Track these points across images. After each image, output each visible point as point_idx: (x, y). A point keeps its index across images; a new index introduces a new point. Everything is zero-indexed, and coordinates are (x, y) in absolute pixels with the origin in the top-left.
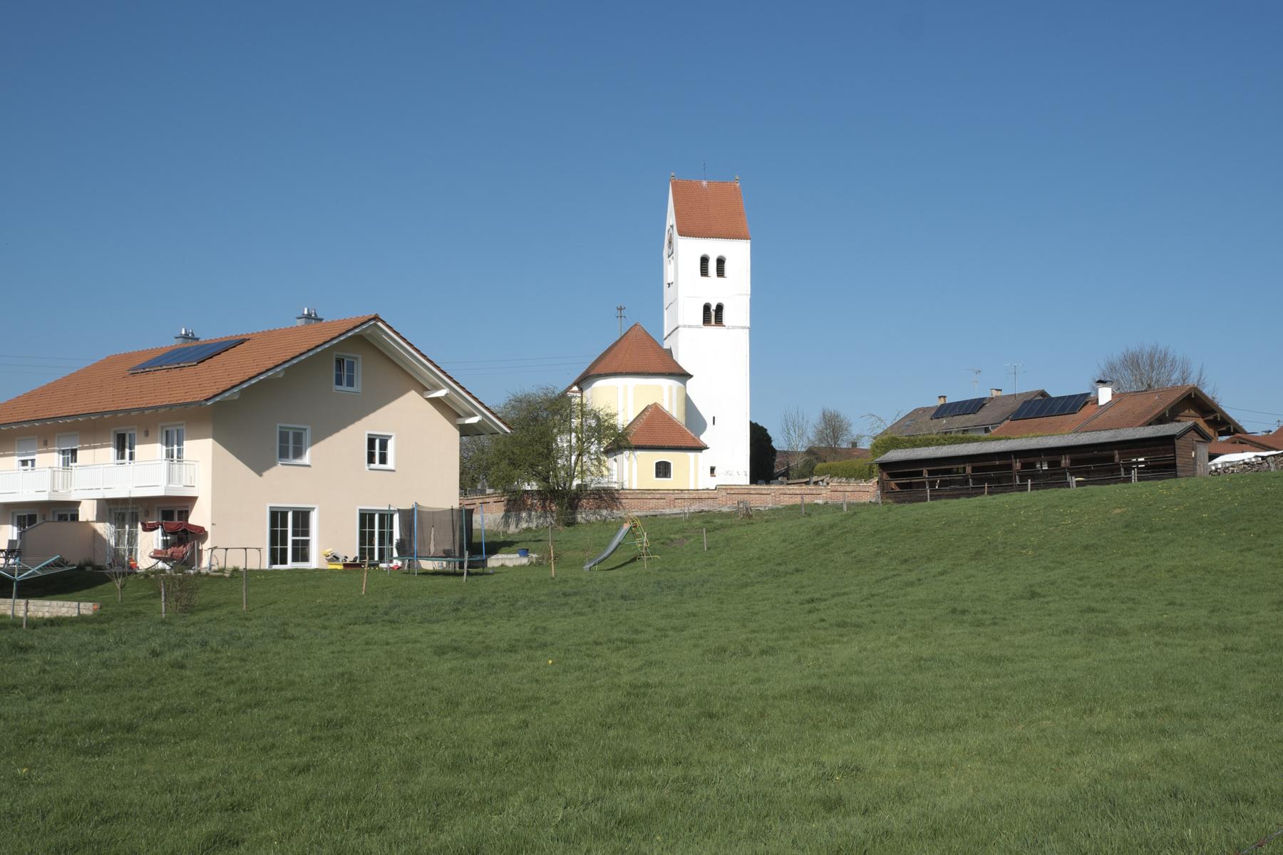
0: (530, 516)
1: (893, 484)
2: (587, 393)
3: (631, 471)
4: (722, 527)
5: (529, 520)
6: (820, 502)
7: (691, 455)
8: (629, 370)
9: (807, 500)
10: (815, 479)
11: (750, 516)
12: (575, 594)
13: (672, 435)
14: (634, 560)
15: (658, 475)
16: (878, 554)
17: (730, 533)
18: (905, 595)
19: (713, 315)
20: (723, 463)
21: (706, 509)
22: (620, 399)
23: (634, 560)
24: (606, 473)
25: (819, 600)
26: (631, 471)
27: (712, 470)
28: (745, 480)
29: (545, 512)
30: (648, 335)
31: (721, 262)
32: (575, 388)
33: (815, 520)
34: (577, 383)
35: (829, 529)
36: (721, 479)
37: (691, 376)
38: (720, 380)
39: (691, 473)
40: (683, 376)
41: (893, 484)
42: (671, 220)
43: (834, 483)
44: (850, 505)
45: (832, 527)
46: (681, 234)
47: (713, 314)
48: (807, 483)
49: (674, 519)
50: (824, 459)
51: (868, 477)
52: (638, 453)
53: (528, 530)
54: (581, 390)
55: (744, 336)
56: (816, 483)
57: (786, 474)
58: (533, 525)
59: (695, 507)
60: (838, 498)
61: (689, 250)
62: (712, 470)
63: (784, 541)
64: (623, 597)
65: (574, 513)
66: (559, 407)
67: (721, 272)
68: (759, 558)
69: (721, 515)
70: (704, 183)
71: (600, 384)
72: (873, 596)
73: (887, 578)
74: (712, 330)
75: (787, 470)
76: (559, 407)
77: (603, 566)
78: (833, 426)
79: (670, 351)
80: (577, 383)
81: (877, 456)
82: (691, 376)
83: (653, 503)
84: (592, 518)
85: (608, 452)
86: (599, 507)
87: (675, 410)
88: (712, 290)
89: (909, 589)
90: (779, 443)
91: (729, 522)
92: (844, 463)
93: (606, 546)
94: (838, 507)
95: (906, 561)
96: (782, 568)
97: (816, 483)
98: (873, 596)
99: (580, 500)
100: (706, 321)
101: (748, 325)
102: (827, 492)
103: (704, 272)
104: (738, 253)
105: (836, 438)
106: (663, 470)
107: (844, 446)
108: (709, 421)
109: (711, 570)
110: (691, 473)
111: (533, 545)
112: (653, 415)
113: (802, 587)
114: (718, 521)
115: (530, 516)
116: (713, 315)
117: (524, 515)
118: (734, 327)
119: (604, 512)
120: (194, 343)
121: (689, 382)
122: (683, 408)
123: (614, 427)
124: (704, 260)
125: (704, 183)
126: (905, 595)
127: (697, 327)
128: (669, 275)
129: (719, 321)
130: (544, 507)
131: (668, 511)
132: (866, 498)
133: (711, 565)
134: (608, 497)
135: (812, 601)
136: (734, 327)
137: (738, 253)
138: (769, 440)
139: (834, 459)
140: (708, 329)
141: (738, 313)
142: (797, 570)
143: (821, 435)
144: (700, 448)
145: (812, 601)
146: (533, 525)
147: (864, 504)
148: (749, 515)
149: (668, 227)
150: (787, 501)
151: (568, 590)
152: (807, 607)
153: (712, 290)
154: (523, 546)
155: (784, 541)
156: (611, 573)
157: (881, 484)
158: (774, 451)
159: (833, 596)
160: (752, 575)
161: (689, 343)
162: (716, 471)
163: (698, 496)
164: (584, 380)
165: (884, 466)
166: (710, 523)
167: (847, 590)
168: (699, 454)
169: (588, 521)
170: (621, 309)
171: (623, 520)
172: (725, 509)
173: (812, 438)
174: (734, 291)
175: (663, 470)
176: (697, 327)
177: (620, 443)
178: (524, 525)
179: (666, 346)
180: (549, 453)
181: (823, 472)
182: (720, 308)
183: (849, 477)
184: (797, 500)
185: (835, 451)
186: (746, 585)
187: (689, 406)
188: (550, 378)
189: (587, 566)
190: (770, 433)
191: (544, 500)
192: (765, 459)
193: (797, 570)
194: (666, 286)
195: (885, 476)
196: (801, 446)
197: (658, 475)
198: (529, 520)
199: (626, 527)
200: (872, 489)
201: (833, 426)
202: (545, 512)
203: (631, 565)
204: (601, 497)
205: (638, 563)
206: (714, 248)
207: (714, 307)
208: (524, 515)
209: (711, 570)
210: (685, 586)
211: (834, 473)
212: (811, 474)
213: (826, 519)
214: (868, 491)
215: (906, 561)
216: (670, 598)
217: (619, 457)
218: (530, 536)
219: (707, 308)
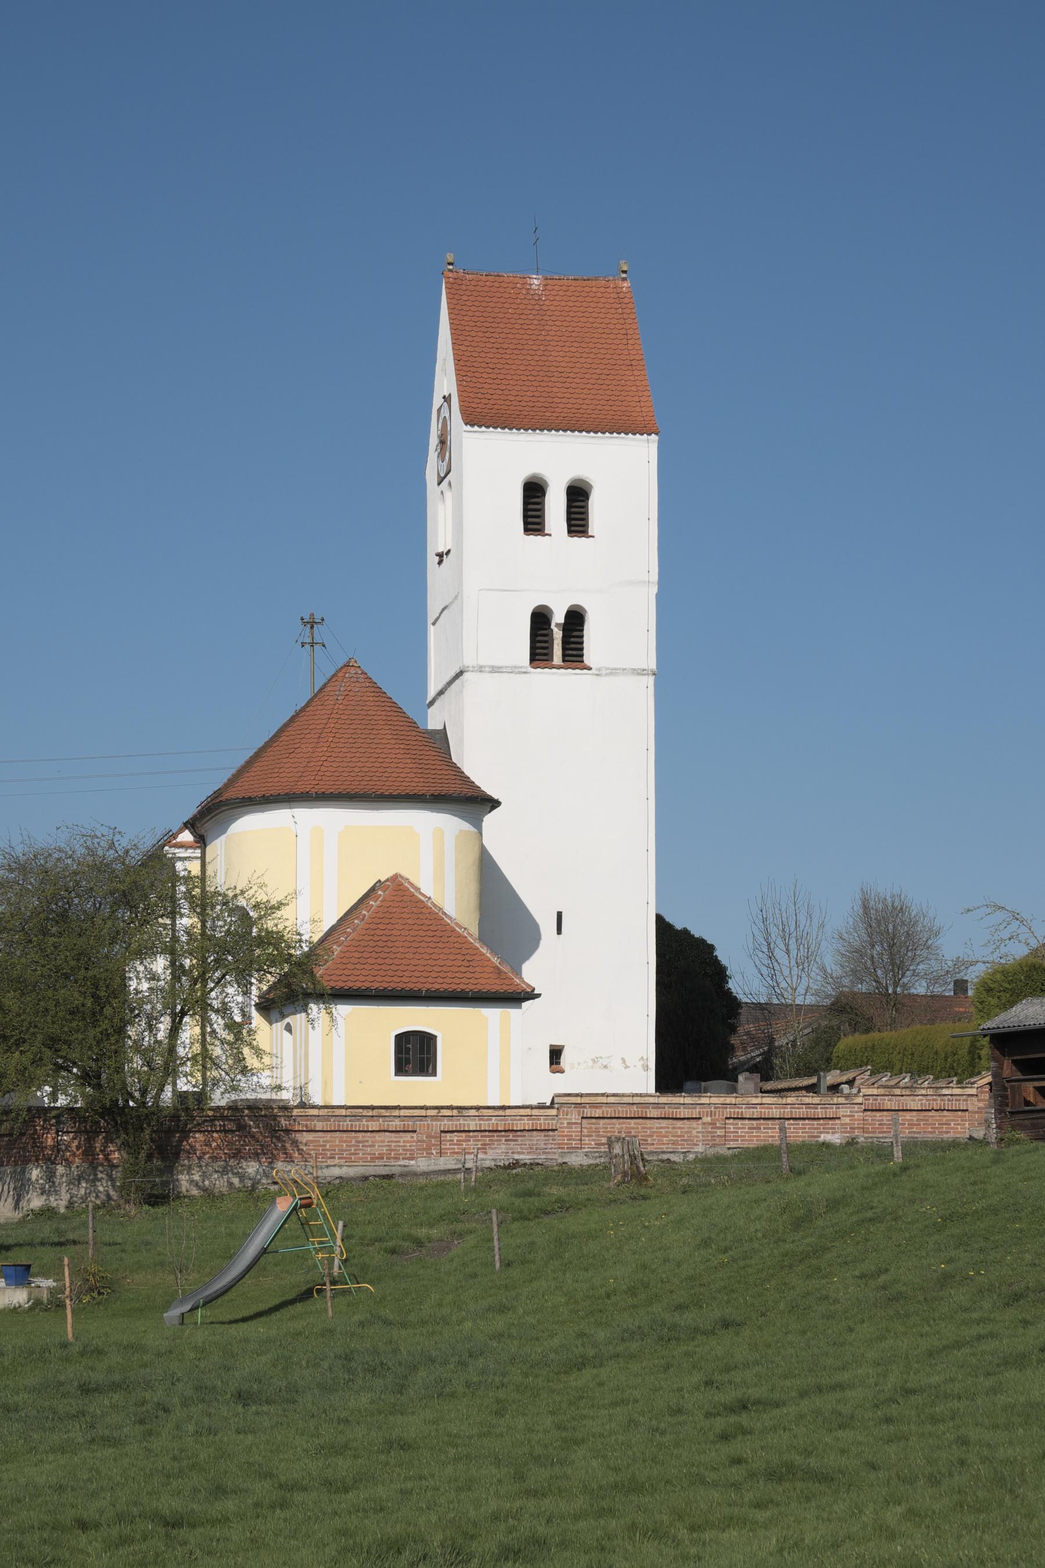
0: (50, 1176)
1: (1029, 1090)
2: (216, 848)
3: (329, 1060)
4: (564, 1206)
5: (50, 1187)
6: (835, 1138)
7: (492, 1015)
8: (321, 789)
9: (798, 1133)
10: (832, 1077)
11: (641, 1178)
12: (115, 1387)
13: (437, 961)
14: (306, 1295)
15: (401, 1069)
16: (945, 1279)
17: (572, 1223)
18: (994, 1391)
19: (557, 638)
20: (587, 1028)
21: (525, 1158)
22: (301, 864)
23: (306, 1295)
24: (252, 1061)
25: (763, 1404)
26: (329, 1060)
27: (556, 1054)
28: (645, 1082)
29: (93, 1165)
30: (379, 692)
31: (578, 495)
32: (187, 836)
33: (794, 1188)
34: (191, 825)
35: (822, 1213)
36: (578, 1078)
37: (494, 804)
38: (579, 814)
39: (489, 1061)
40: (475, 803)
41: (1029, 1090)
42: (445, 381)
43: (869, 1089)
44: (911, 1147)
45: (834, 1205)
46: (473, 418)
47: (558, 634)
48: (812, 1089)
49: (438, 1185)
50: (869, 1020)
51: (956, 1068)
52: (343, 1010)
53: (47, 1213)
54: (202, 841)
55: (640, 699)
56: (834, 1088)
57: (764, 1070)
58: (60, 1202)
59: (498, 1153)
60: (879, 1129)
61: (491, 464)
62: (556, 1054)
63: (706, 1243)
64: (242, 1397)
65: (169, 1170)
66: (140, 886)
67: (578, 522)
68: (632, 1291)
69: (565, 1174)
70: (536, 281)
71: (252, 828)
72: (908, 1392)
73: (958, 1345)
74: (556, 680)
75: (767, 1057)
76: (140, 886)
77: (222, 1311)
78: (889, 935)
79: (442, 735)
80: (191, 825)
81: (989, 1016)
82: (494, 804)
83: (381, 1143)
84: (219, 1183)
85: (269, 1007)
86: (238, 1155)
87: (450, 894)
88: (556, 571)
89: (1011, 1374)
90: (746, 982)
91: (583, 1192)
92: (905, 1035)
93: (230, 1256)
94: (880, 1152)
95: (1017, 1297)
96: (687, 1318)
97: (834, 1088)
98: (908, 1392)
99: (186, 1134)
100: (539, 654)
101: (653, 665)
102: (853, 1113)
103: (533, 521)
104: (623, 469)
105: (898, 968)
106: (415, 1054)
107: (920, 989)
108: (547, 925)
109: (500, 1323)
110: (489, 1061)
111: (47, 1254)
112: (391, 909)
113: (728, 1369)
114: (556, 1191)
115: (50, 1176)
116: (557, 638)
117: (35, 1173)
118: (613, 672)
119: (252, 1168)
120: (430, 620)
121: (490, 820)
122: (472, 888)
123: (273, 939)
124: (534, 492)
125: (536, 281)
126: (994, 1391)
127: (514, 670)
128: (440, 534)
129: (575, 654)
130: (89, 1153)
131: (422, 1164)
132: (960, 1129)
133: (503, 1309)
134: (265, 1127)
135: (743, 1406)
136: (613, 672)
137: (623, 469)
138: (720, 973)
139: (893, 1024)
140: (544, 677)
141: (624, 633)
142: (726, 1324)
143: (858, 959)
144: (518, 997)
145: (743, 1406)
146: (60, 1202)
147: (955, 1144)
148: (637, 1176)
149: (437, 401)
150: (748, 1137)
151: (98, 1377)
152: (719, 1424)
153: (556, 571)
154: (21, 1257)
155: (706, 1243)
156: (233, 1329)
157: (1000, 1090)
158: (732, 1004)
159: (803, 1394)
160: (602, 1335)
161: (493, 714)
162: (565, 1059)
163: (501, 1122)
164: (209, 818)
165: (1005, 1042)
166: (536, 1194)
167: (845, 1377)
168: (512, 1013)
169: (209, 1194)
170: (312, 624)
171: (283, 1187)
172: (576, 1160)
173: (838, 971)
174: (615, 574)
175: (415, 1054)
176: (514, 670)
177: (299, 985)
178: (36, 1202)
179: (433, 721)
180: (105, 1006)
181: (855, 1061)
182: (575, 619)
183: (919, 1071)
184: (770, 1135)
185: (898, 1006)
186: (581, 1364)
187: (489, 876)
188: (133, 815)
189: (174, 1313)
190: (722, 955)
191: (91, 1134)
192: (699, 1018)
193: (726, 1324)
194: (432, 560)
195: (1008, 1069)
196: (806, 989)
197: (401, 1069)
198: (50, 1187)
199: (283, 1206)
200: (974, 1105)
201: (889, 935)
202: (93, 1165)
203: (299, 1307)
204: (241, 1127)
205: (315, 1303)
206: (559, 456)
207: (559, 617)
208: (35, 1173)
209: (500, 1323)
210: (414, 1368)
211: (882, 1063)
212: (828, 1064)
213: (821, 1185)
214: (963, 1110)
215: (1017, 1297)
216: (365, 1399)
217: (297, 1020)
218: (46, 1231)
219: (540, 619)
